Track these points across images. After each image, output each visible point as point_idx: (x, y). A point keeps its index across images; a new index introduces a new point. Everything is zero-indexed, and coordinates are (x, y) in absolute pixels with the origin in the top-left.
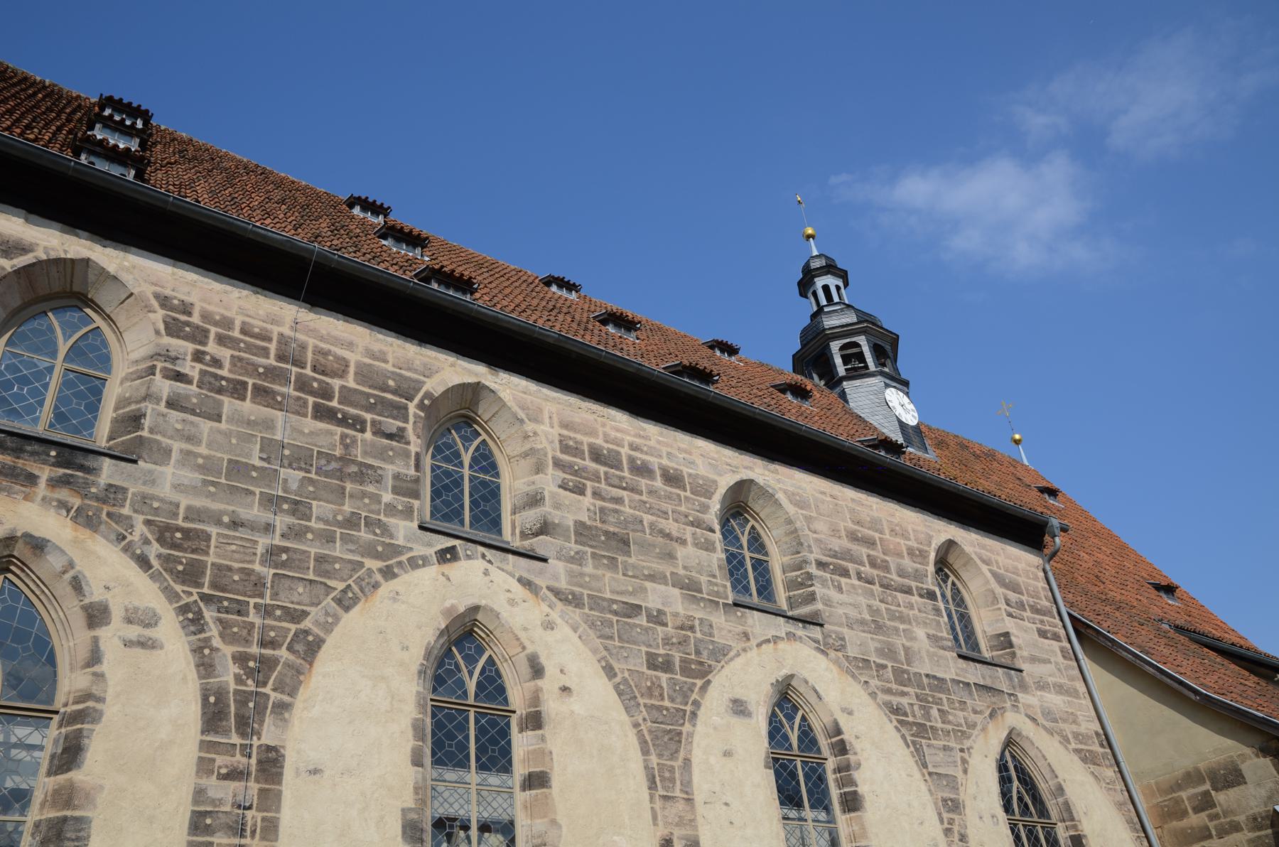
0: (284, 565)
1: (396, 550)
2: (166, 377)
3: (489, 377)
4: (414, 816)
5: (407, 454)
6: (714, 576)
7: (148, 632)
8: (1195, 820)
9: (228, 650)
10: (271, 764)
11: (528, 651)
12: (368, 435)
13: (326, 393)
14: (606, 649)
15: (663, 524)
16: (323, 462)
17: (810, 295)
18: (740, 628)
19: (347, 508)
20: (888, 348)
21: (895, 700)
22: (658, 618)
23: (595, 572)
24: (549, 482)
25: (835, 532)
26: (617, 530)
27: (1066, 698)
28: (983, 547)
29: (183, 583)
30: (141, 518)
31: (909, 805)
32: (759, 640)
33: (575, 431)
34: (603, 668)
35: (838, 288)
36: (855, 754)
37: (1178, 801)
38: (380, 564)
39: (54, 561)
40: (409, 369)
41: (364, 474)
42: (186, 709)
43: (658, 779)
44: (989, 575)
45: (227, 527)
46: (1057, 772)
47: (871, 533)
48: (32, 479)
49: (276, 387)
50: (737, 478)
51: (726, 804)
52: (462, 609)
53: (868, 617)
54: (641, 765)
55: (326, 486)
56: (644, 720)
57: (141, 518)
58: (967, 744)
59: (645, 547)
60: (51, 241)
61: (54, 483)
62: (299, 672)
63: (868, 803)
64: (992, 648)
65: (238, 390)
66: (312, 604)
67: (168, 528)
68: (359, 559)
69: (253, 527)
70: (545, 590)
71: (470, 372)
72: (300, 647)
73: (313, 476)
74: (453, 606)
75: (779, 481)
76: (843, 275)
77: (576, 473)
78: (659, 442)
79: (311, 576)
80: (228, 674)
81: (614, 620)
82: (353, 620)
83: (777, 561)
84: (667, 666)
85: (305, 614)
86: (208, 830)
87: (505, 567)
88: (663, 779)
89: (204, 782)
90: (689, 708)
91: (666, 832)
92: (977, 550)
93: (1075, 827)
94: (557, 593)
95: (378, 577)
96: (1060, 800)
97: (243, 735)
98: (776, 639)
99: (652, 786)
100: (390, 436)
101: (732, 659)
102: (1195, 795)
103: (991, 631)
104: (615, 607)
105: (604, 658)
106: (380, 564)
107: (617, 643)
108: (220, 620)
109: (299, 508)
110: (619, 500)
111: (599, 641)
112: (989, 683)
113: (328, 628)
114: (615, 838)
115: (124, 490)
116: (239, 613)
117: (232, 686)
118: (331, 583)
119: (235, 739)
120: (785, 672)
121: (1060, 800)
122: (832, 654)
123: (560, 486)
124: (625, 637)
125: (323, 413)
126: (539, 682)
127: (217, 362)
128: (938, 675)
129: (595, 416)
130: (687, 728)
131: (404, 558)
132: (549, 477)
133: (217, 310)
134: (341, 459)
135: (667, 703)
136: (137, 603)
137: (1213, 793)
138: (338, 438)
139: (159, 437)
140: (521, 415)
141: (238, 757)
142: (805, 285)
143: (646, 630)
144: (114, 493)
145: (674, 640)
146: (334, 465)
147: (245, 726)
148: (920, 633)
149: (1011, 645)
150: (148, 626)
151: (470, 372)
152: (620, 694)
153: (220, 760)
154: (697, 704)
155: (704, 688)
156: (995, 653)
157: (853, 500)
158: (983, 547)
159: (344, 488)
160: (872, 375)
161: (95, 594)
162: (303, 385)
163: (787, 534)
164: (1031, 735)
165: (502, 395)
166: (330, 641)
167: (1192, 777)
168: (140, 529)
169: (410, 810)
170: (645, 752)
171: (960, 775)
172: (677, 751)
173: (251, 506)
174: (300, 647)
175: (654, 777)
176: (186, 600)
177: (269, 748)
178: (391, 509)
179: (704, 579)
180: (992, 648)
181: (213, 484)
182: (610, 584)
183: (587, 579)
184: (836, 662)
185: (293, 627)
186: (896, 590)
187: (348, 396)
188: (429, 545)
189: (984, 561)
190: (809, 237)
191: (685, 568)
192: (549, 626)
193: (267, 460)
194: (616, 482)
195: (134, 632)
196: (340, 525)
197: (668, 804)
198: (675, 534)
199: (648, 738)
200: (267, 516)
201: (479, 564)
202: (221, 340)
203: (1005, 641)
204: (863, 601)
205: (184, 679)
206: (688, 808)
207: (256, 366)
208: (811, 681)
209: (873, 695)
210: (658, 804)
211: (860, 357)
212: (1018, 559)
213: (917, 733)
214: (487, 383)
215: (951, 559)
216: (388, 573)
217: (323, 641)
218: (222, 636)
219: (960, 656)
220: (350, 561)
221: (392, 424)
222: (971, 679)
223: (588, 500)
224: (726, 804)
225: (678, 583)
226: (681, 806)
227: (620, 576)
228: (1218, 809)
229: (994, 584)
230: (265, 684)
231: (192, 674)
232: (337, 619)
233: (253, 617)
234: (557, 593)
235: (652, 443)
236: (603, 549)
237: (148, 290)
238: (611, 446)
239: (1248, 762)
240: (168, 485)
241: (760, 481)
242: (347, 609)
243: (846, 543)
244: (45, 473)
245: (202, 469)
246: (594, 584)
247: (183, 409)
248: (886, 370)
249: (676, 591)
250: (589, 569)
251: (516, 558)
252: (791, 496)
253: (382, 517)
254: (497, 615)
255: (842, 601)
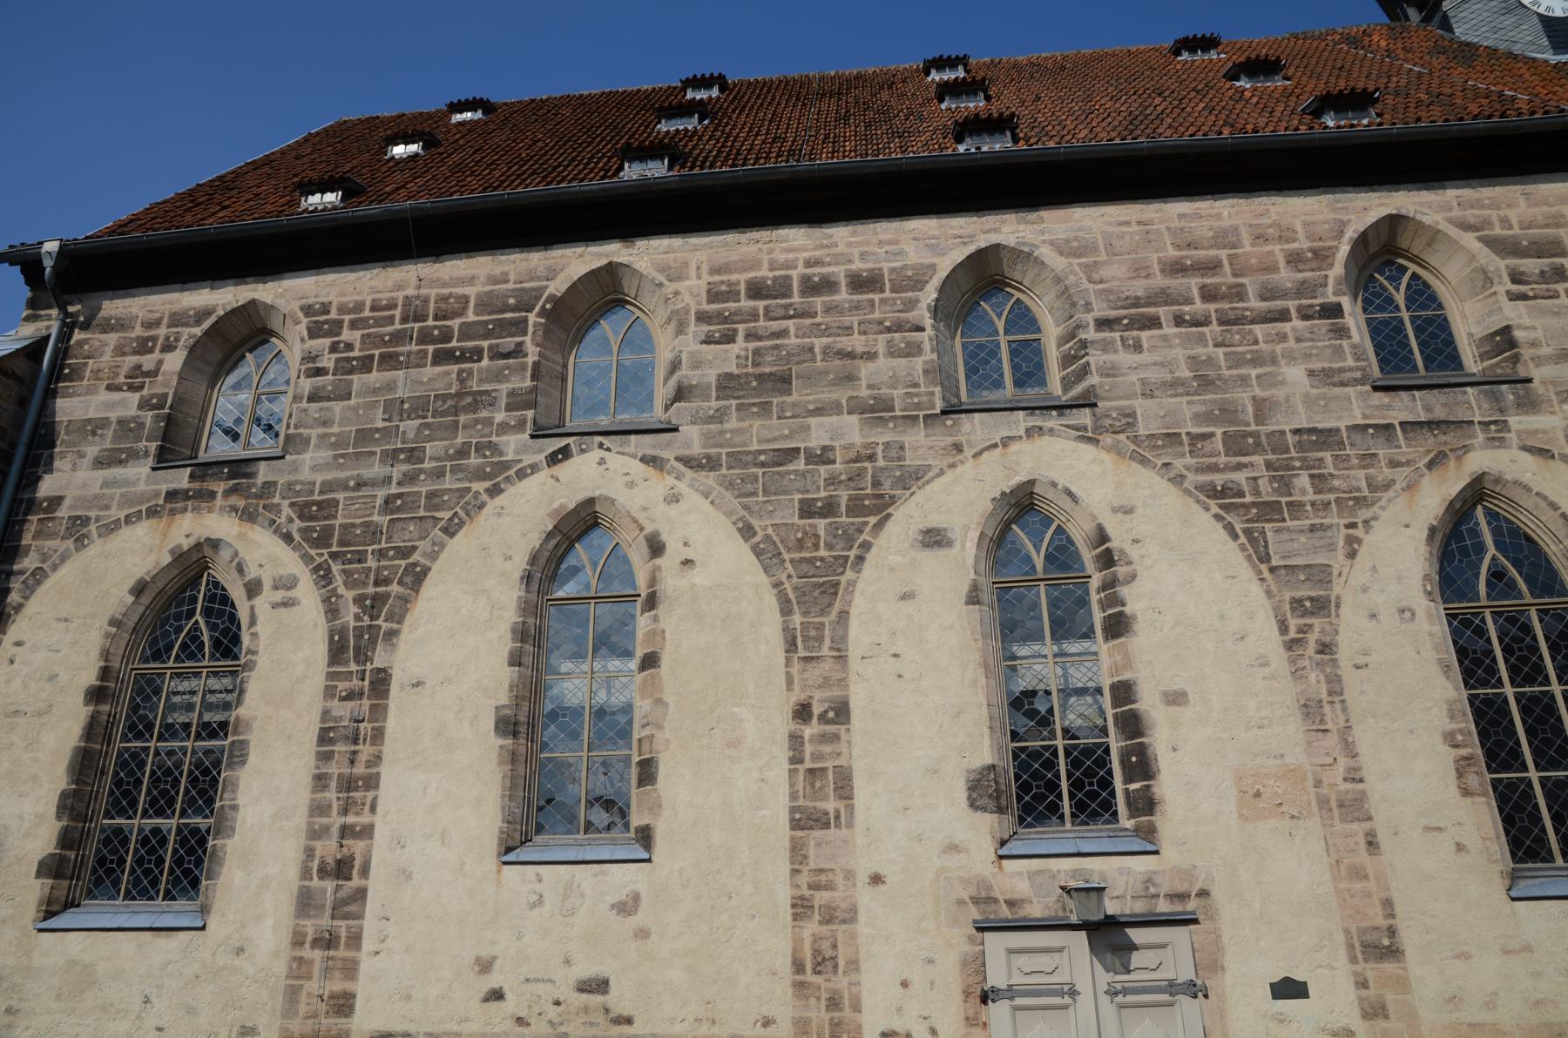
0: (398, 510)
1: (505, 466)
2: (308, 376)
3: (624, 252)
4: (508, 712)
5: (523, 367)
6: (916, 385)
7: (290, 594)
9: (349, 595)
10: (381, 683)
11: (647, 531)
12: (485, 362)
13: (446, 336)
14: (745, 507)
15: (844, 343)
16: (439, 403)
18: (950, 440)
19: (459, 440)
21: (1219, 479)
22: (823, 456)
23: (740, 425)
24: (689, 344)
25: (1141, 270)
26: (774, 369)
29: (317, 547)
30: (287, 502)
31: (1222, 617)
32: (977, 449)
33: (730, 272)
34: (739, 530)
36: (1129, 563)
38: (487, 484)
39: (225, 554)
40: (532, 279)
41: (482, 400)
42: (317, 648)
43: (799, 640)
45: (353, 489)
48: (213, 495)
49: (400, 349)
50: (972, 249)
51: (895, 655)
52: (571, 506)
54: (778, 627)
55: (441, 426)
56: (789, 576)
57: (287, 502)
58: (1364, 514)
59: (810, 378)
60: (224, 297)
61: (228, 493)
62: (407, 601)
63: (1140, 626)
64: (1483, 357)
65: (365, 365)
66: (422, 538)
67: (308, 504)
68: (467, 485)
69: (373, 483)
70: (673, 462)
71: (599, 255)
72: (408, 580)
73: (429, 420)
74: (562, 506)
75: (1042, 232)
77: (725, 320)
78: (849, 245)
79: (422, 513)
80: (350, 615)
81: (746, 475)
82: (459, 544)
83: (1051, 333)
84: (829, 509)
85: (414, 548)
86: (332, 741)
87: (627, 450)
88: (806, 638)
89: (329, 704)
90: (852, 553)
91: (803, 696)
94: (687, 461)
95: (485, 497)
97: (357, 662)
98: (1006, 442)
99: (791, 646)
100: (507, 356)
101: (929, 482)
103: (1480, 331)
104: (762, 458)
105: (742, 519)
106: (487, 484)
107: (761, 498)
108: (344, 571)
109: (414, 455)
110: (783, 333)
111: (736, 501)
112: (1440, 414)
113: (434, 556)
114: (736, 710)
115: (275, 483)
116: (360, 561)
117: (352, 624)
118: (438, 515)
119: (353, 667)
120: (1021, 478)
122: (1108, 439)
123: (703, 342)
124: (773, 489)
125: (442, 357)
126: (658, 561)
127: (349, 347)
128: (1320, 426)
129: (760, 245)
130: (849, 574)
131: (512, 472)
132: (690, 336)
133: (349, 299)
134: (457, 394)
135: (823, 553)
136: (282, 572)
138: (454, 376)
139: (301, 431)
140: (660, 278)
141: (355, 681)
143: (803, 474)
144: (269, 486)
145: (843, 477)
146: (449, 403)
147: (362, 656)
148: (1295, 374)
149: (1512, 344)
150: (290, 588)
151: (599, 255)
152: (758, 555)
153: (342, 686)
154: (866, 546)
155: (879, 526)
156: (1487, 363)
157: (1181, 216)
159: (457, 422)
161: (252, 573)
162: (425, 337)
163: (1058, 297)
164: (1527, 478)
165: (637, 266)
166: (435, 568)
168: (287, 511)
169: (503, 706)
170: (786, 610)
171: (1338, 560)
172: (830, 605)
173: (373, 465)
174: (408, 580)
175: (795, 638)
176: (319, 560)
177: (380, 670)
178: (504, 428)
179: (897, 393)
180: (1483, 357)
181: (342, 456)
182: (758, 433)
183: (728, 436)
184: (1116, 450)
185: (403, 563)
186: (1252, 322)
187: (467, 332)
188: (540, 451)
189: (1466, 227)
191: (870, 387)
192: (674, 498)
193: (389, 420)
194: (781, 312)
195: (279, 596)
196: (451, 458)
197: (809, 666)
198: (859, 349)
199: (792, 596)
200: (385, 470)
201: (597, 454)
202: (354, 325)
203: (1503, 341)
204: (1180, 354)
205: (315, 625)
206: (838, 667)
207: (382, 336)
208: (1061, 483)
209: (1178, 480)
210: (796, 667)
213: (1251, 518)
214: (620, 260)
216: (495, 491)
217: (429, 569)
218: (345, 584)
219: (1376, 388)
220: (458, 490)
221: (509, 342)
222: (1396, 417)
223: (739, 346)
224: (895, 655)
225: (857, 407)
226: (827, 665)
227: (775, 421)
229: (1485, 256)
230: (378, 617)
231: (322, 620)
232: (443, 546)
233: (371, 563)
234: (687, 461)
235: (841, 249)
236: (753, 396)
237: (295, 306)
238: (777, 273)
240: (307, 470)
241: (1011, 241)
242: (452, 535)
243: (1159, 281)
244: (220, 487)
245: (334, 446)
246: (736, 439)
247: (321, 399)
249: (855, 418)
250: (732, 423)
251: (639, 437)
252: (1063, 249)
253: (494, 439)
254: (613, 502)
255: (1135, 370)
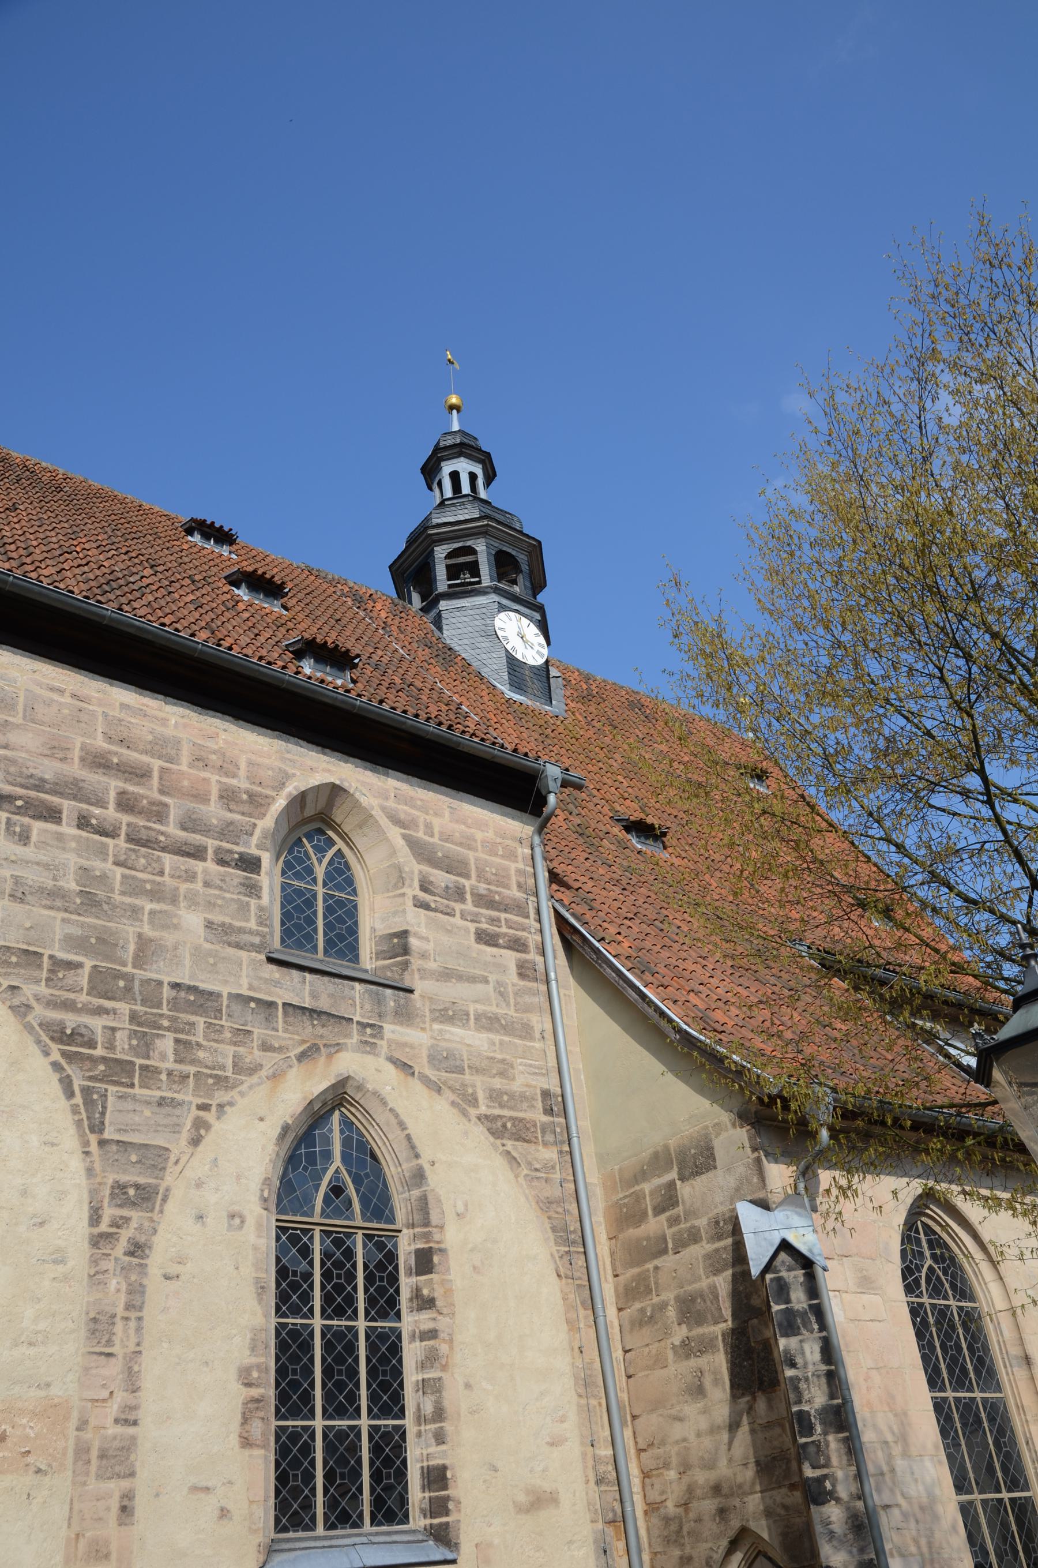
8: (654, 1225)
17: (435, 486)
20: (522, 558)
21: (71, 1020)
27: (496, 1038)
28: (409, 802)
35: (473, 477)
37: (638, 1197)
44: (400, 843)
46: (420, 1149)
47: (145, 759)
53: (73, 886)
76: (486, 460)
92: (391, 804)
93: (427, 1237)
96: (416, 1193)
102: (659, 1188)
103: (384, 928)
121: (416, 1193)
128: (202, 986)
137: (678, 1183)
142: (430, 471)
148: (193, 921)
149: (406, 950)
157: (124, 706)
158: (409, 802)
160: (483, 592)
164: (386, 1091)
167: (659, 1161)
180: (380, 955)
186: (164, 849)
190: (452, 407)
203: (399, 944)
211: (474, 569)
212: (482, 825)
215: (338, 815)
228: (680, 1210)
239: (724, 1135)
248: (516, 589)
